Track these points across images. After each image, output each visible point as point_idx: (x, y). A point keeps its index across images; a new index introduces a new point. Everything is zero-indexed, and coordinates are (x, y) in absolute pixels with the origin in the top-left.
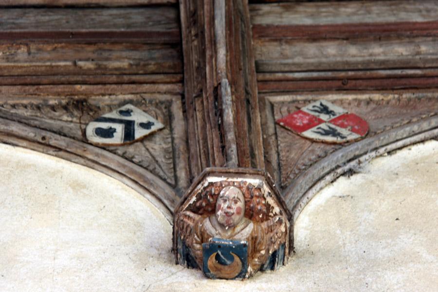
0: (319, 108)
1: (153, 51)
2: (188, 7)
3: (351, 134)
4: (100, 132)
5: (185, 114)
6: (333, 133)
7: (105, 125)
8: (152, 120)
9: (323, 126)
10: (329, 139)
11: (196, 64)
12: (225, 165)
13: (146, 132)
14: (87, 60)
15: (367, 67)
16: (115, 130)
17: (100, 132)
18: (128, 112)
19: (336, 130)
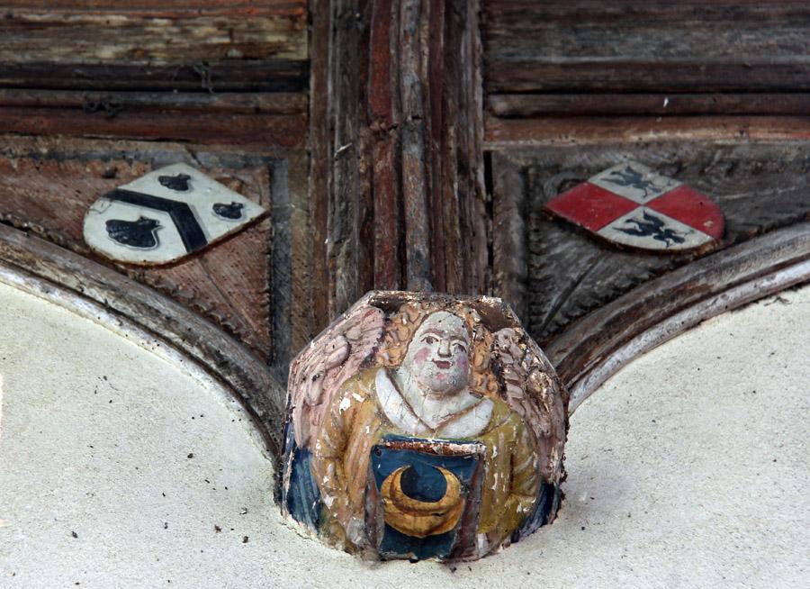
0: (624, 176)
1: (448, 288)
2: (470, 118)
3: (692, 232)
4: (120, 230)
5: (634, 146)
6: (653, 227)
7: (130, 213)
8: (239, 199)
9: (638, 214)
10: (650, 242)
11: (302, 388)
12: (519, 26)
13: (232, 225)
14: (162, 18)
15: (744, 114)
16: (153, 224)
17: (120, 230)
18: (181, 183)
19: (662, 224)
